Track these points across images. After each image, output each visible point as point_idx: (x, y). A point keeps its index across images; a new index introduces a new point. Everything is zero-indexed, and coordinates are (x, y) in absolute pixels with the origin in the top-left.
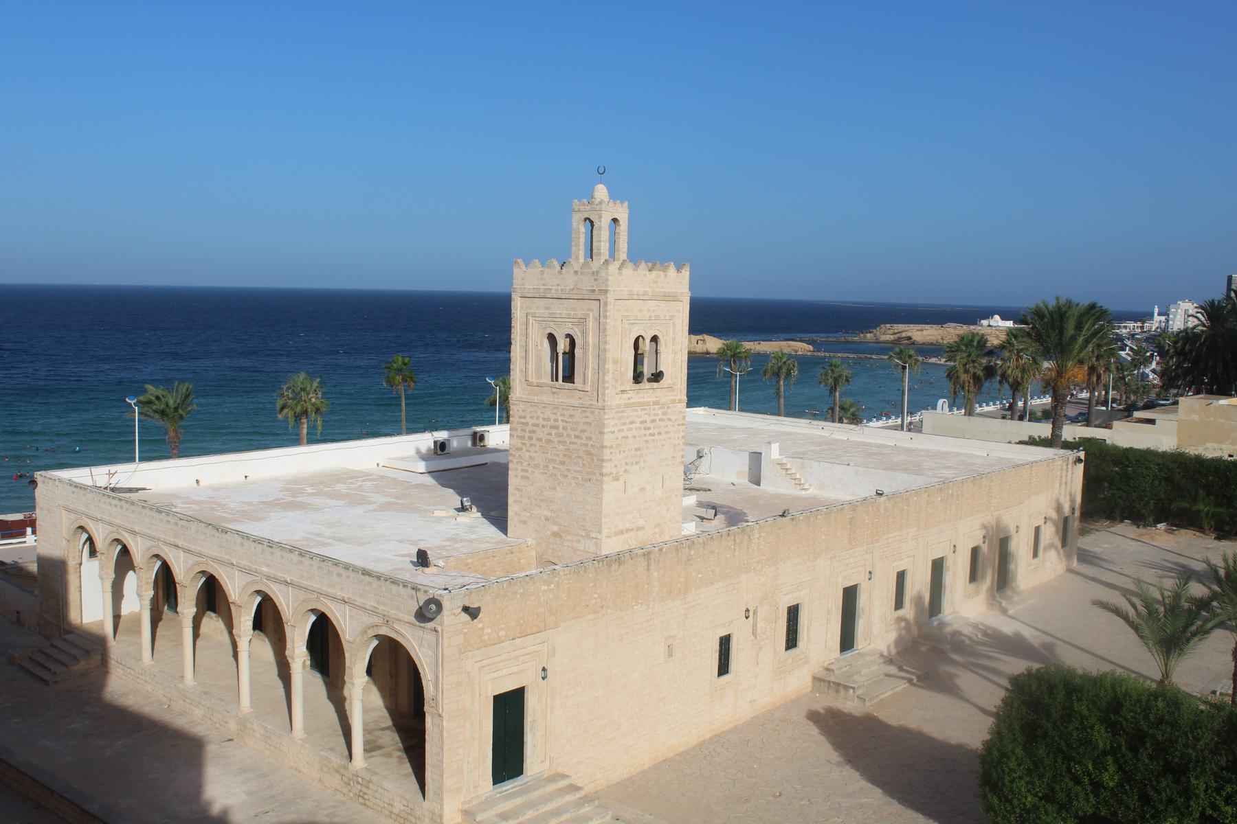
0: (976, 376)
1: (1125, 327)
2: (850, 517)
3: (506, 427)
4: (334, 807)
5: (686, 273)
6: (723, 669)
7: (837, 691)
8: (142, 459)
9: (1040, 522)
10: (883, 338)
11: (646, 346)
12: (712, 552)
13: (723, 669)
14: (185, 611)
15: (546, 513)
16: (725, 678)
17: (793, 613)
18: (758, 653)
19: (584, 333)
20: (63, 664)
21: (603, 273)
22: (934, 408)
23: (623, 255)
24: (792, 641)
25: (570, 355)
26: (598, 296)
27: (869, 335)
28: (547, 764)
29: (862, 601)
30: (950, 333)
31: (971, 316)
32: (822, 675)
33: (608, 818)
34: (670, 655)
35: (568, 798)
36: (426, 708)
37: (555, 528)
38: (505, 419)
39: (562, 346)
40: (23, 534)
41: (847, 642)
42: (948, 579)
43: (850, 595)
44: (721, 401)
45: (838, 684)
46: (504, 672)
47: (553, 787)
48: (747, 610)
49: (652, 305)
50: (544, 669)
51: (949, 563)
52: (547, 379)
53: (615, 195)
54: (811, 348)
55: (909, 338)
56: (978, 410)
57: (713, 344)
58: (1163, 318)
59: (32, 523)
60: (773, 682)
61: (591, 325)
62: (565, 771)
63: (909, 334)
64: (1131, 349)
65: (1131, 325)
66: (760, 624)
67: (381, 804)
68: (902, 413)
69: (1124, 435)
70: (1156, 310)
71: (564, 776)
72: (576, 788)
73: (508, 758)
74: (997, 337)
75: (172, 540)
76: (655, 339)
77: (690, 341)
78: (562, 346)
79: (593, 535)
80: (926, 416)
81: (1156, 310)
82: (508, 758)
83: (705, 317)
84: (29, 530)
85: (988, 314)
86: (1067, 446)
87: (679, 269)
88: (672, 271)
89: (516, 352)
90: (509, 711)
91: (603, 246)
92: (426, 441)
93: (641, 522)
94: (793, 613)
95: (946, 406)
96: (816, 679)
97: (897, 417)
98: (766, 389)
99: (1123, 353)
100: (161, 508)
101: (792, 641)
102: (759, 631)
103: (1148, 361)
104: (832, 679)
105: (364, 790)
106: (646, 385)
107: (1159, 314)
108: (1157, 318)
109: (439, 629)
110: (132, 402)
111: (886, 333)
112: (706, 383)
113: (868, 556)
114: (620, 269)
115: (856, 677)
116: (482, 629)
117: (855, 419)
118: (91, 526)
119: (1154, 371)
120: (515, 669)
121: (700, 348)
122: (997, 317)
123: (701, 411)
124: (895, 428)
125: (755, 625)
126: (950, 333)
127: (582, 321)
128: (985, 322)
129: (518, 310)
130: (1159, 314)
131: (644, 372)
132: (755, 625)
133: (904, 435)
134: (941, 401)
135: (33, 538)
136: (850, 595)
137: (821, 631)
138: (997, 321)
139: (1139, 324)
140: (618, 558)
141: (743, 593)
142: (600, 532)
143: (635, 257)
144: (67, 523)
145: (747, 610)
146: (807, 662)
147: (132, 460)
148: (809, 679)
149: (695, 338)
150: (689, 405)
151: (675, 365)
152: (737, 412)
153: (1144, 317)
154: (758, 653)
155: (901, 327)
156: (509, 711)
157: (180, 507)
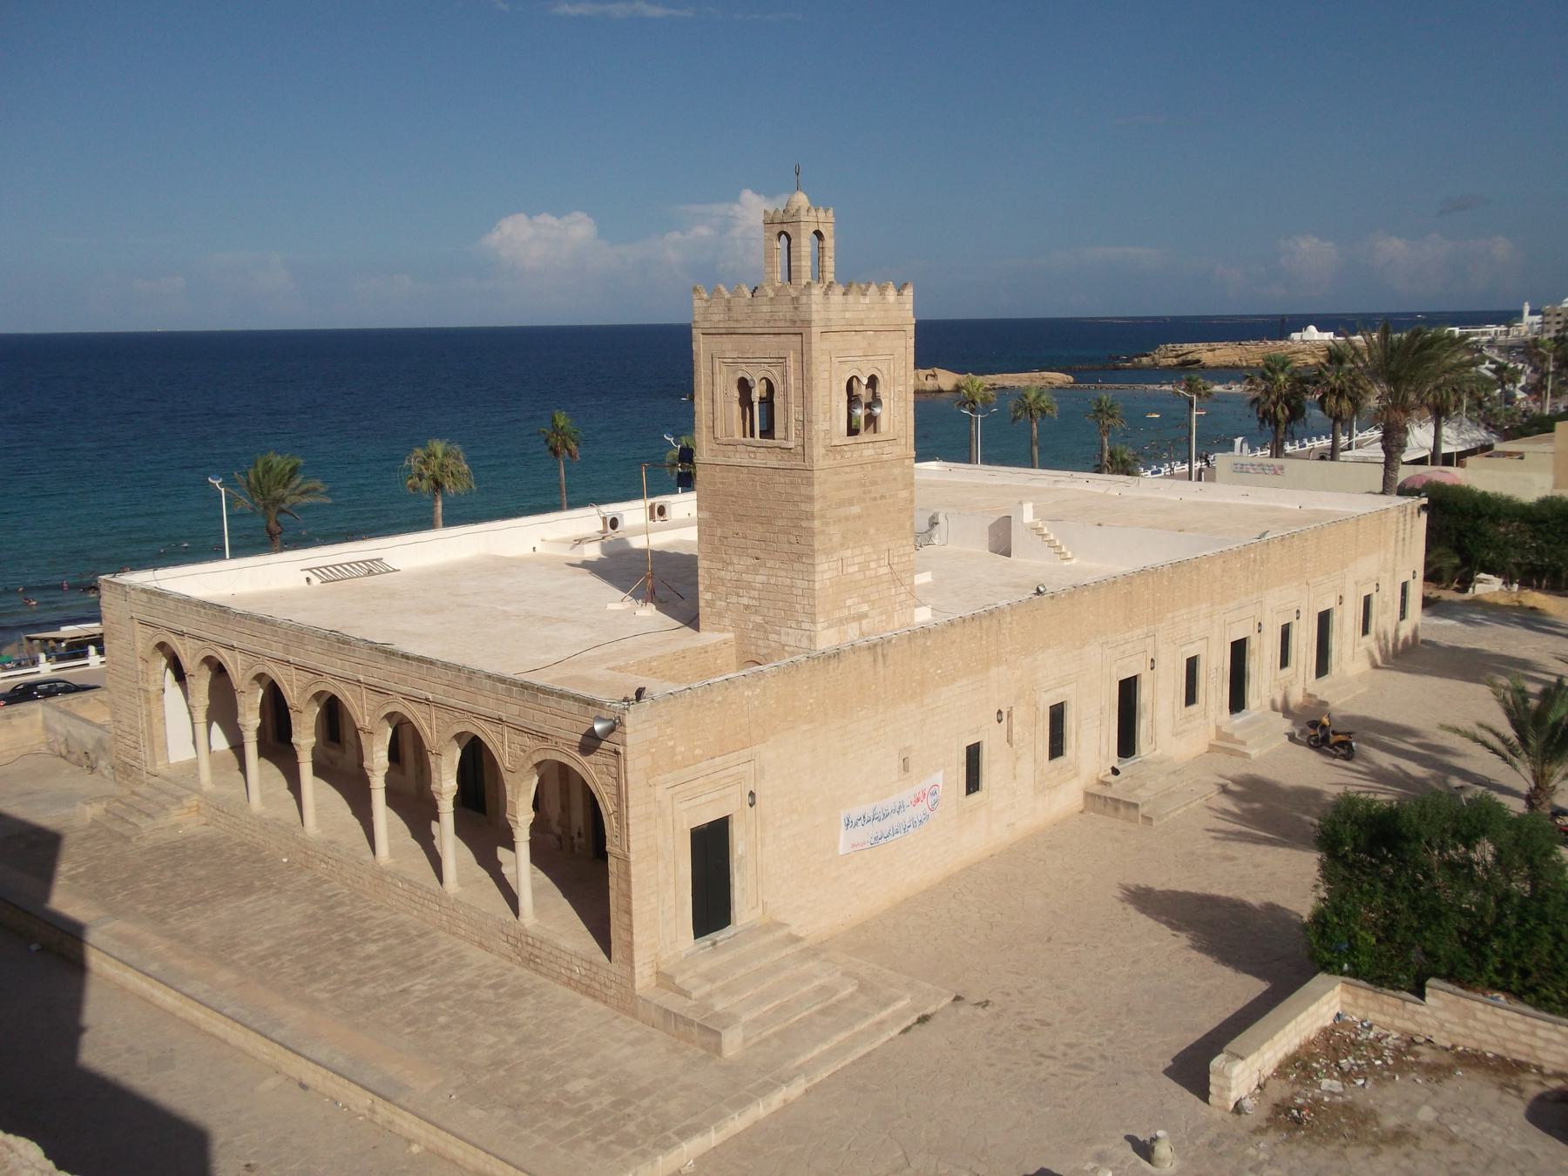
0: (1285, 412)
2: (1134, 593)
3: (692, 496)
4: (498, 975)
5: (909, 293)
6: (973, 784)
7: (1117, 809)
8: (232, 557)
9: (1407, 576)
10: (1164, 362)
11: (863, 392)
13: (973, 784)
14: (302, 742)
15: (745, 601)
16: (976, 796)
17: (1057, 715)
18: (1016, 763)
19: (784, 376)
20: (148, 815)
21: (804, 299)
22: (1231, 447)
24: (1057, 747)
25: (768, 402)
26: (799, 329)
27: (1145, 360)
28: (759, 911)
29: (1144, 695)
30: (1250, 353)
31: (1283, 326)
32: (1097, 789)
33: (838, 974)
34: (906, 769)
35: (790, 950)
36: (608, 847)
37: (759, 619)
39: (757, 392)
40: (85, 655)
41: (1127, 745)
42: (1253, 665)
43: (1128, 689)
44: (958, 452)
45: (1117, 801)
46: (703, 799)
47: (768, 938)
48: (1000, 712)
49: (866, 335)
50: (752, 794)
51: (1252, 646)
52: (738, 436)
53: (815, 204)
54: (1071, 379)
55: (1198, 361)
56: (1288, 448)
57: (946, 379)
58: (1537, 318)
59: (98, 642)
60: (1033, 798)
61: (791, 363)
62: (781, 918)
63: (1196, 356)
65: (1492, 329)
66: (1016, 729)
67: (557, 968)
68: (1190, 457)
69: (1480, 477)
70: (1527, 308)
71: (781, 925)
72: (796, 940)
73: (712, 905)
74: (1313, 355)
75: (280, 655)
76: (873, 381)
77: (917, 376)
78: (757, 392)
79: (805, 626)
80: (1220, 460)
81: (1527, 308)
82: (712, 905)
83: (936, 343)
84: (92, 649)
85: (1300, 323)
86: (1403, 491)
89: (702, 405)
90: (711, 848)
91: (805, 264)
92: (584, 521)
93: (865, 608)
94: (1057, 715)
95: (1245, 446)
96: (1089, 796)
97: (1183, 463)
98: (1017, 440)
100: (219, 611)
101: (1057, 747)
102: (1015, 737)
103: (1514, 377)
104: (1109, 794)
105: (536, 952)
106: (864, 436)
107: (1532, 313)
108: (1527, 318)
109: (621, 750)
110: (217, 483)
111: (1166, 355)
112: (939, 434)
113: (1149, 641)
115: (1139, 792)
116: (673, 747)
118: (176, 644)
119: (1523, 389)
120: (716, 795)
121: (930, 384)
122: (1312, 328)
123: (933, 466)
124: (1180, 477)
125: (1010, 731)
126: (1250, 353)
128: (1296, 336)
132: (1010, 731)
133: (1194, 485)
134: (1238, 441)
135: (98, 659)
136: (1128, 689)
137: (1093, 733)
138: (1312, 333)
139: (1503, 328)
140: (837, 654)
141: (984, 701)
142: (814, 622)
144: (143, 640)
145: (1000, 712)
146: (1076, 775)
147: (224, 558)
148: (1081, 796)
149: (923, 373)
151: (897, 415)
152: (979, 466)
153: (1509, 317)
154: (1016, 763)
155: (1187, 347)
156: (711, 848)
157: (239, 608)
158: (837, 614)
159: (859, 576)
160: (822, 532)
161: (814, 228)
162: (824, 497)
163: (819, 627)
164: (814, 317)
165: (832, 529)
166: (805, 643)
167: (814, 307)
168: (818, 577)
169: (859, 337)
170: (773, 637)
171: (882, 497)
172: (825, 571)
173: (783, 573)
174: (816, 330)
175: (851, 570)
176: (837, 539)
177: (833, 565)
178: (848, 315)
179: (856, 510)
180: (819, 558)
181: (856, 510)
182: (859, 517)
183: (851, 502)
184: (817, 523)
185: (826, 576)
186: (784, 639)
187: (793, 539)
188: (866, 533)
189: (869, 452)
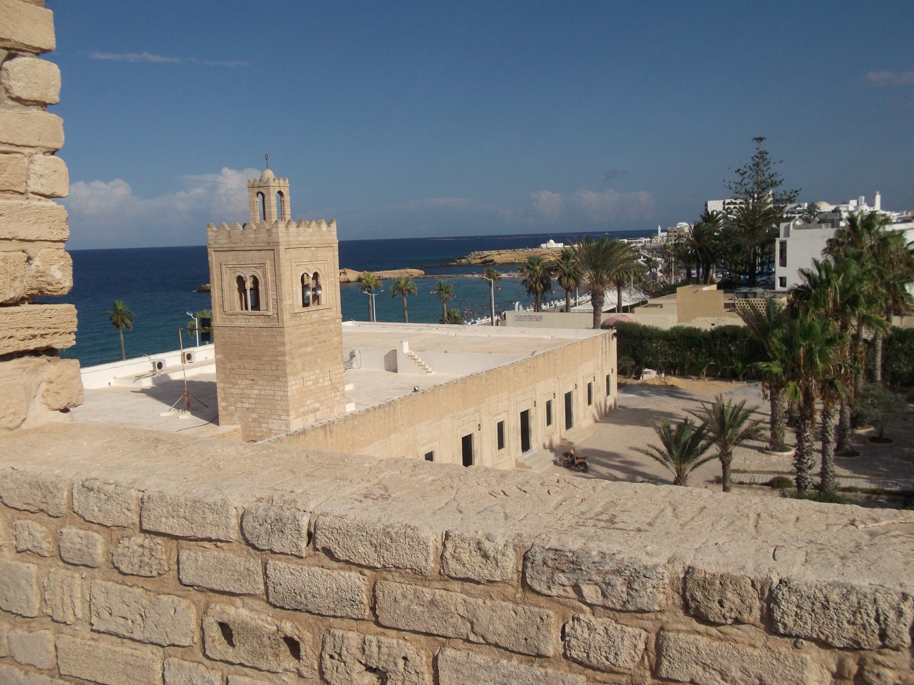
1: (639, 242)
2: (467, 388)
5: (334, 225)
10: (474, 262)
12: (370, 421)
15: (247, 405)
19: (265, 274)
21: (274, 230)
23: (288, 217)
25: (255, 290)
26: (272, 247)
29: (476, 445)
31: (536, 240)
37: (255, 416)
38: (206, 338)
39: (249, 285)
42: (532, 425)
44: (363, 316)
49: (310, 250)
51: (532, 414)
52: (238, 310)
53: (278, 176)
56: (544, 307)
61: (269, 267)
63: (491, 258)
64: (645, 257)
65: (643, 240)
69: (642, 318)
76: (316, 276)
78: (249, 285)
79: (283, 418)
83: (351, 253)
85: (546, 240)
86: (604, 327)
87: (329, 224)
88: (324, 226)
91: (273, 210)
93: (317, 405)
95: (521, 307)
97: (488, 317)
98: (396, 307)
99: (639, 261)
103: (656, 265)
107: (662, 231)
108: (660, 233)
111: (475, 258)
112: (355, 306)
113: (476, 414)
114: (287, 227)
117: (455, 321)
119: (660, 271)
122: (552, 241)
127: (262, 265)
128: (544, 246)
129: (214, 259)
130: (662, 231)
131: (310, 292)
138: (552, 244)
139: (649, 239)
142: (288, 415)
143: (299, 219)
150: (343, 321)
151: (330, 294)
152: (375, 322)
153: (651, 234)
155: (486, 253)
158: (302, 410)
159: (313, 387)
160: (291, 363)
161: (278, 189)
162: (291, 343)
163: (291, 417)
164: (281, 240)
165: (297, 361)
166: (284, 428)
167: (280, 234)
168: (289, 389)
169: (307, 251)
170: (264, 425)
171: (325, 341)
172: (294, 385)
173: (269, 388)
174: (282, 248)
175: (308, 384)
176: (299, 366)
177: (298, 381)
178: (300, 238)
179: (309, 349)
180: (290, 378)
181: (309, 349)
182: (312, 353)
183: (306, 345)
184: (287, 358)
185: (294, 388)
186: (271, 426)
187: (274, 368)
188: (316, 362)
189: (315, 316)
